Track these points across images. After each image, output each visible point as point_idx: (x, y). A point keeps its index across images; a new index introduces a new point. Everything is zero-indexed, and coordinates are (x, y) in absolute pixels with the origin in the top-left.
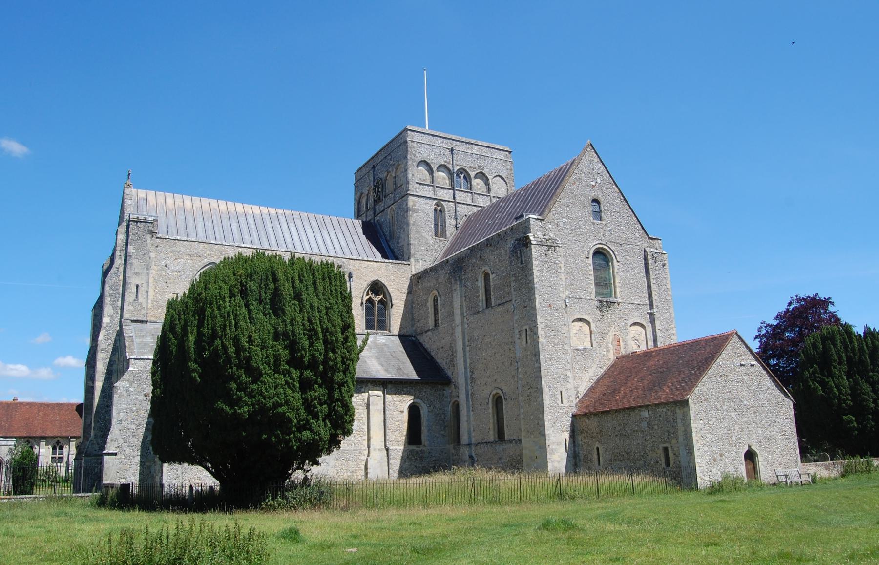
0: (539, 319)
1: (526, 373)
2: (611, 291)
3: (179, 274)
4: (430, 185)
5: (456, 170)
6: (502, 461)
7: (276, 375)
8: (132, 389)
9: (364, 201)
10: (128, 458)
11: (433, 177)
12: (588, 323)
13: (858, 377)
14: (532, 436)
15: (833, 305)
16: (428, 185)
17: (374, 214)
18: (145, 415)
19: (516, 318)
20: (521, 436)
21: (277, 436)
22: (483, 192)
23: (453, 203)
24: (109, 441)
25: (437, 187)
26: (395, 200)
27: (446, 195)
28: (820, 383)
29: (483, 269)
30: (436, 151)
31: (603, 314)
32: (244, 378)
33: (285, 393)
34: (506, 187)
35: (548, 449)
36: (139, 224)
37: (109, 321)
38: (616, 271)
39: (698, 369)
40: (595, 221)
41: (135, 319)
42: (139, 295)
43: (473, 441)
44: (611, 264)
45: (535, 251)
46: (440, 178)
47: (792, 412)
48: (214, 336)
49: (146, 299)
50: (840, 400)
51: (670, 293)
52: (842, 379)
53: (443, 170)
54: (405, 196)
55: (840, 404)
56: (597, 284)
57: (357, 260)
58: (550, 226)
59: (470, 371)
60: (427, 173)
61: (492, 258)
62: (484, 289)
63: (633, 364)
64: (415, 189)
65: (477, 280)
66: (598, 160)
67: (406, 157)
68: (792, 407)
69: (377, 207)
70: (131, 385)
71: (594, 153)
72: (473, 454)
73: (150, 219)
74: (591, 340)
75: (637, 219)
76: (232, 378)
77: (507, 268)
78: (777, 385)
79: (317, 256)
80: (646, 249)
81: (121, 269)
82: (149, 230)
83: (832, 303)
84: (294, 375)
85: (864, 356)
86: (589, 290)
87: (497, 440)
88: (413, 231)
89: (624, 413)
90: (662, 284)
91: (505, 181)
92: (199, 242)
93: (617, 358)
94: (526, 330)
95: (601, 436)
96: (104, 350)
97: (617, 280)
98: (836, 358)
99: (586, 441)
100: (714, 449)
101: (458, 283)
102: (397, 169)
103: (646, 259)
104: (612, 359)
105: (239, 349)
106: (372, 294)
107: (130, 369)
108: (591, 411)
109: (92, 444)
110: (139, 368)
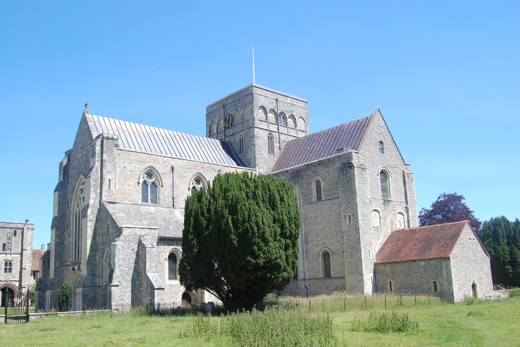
0: (359, 210)
1: (349, 239)
2: (388, 194)
3: (132, 173)
4: (266, 122)
5: (279, 113)
6: (329, 289)
7: (275, 242)
8: (125, 246)
9: (215, 127)
10: (125, 288)
11: (267, 117)
12: (379, 212)
13: (513, 245)
14: (353, 275)
15: (464, 199)
16: (265, 122)
17: (225, 135)
18: (133, 262)
19: (342, 208)
20: (345, 275)
21: (275, 275)
22: (292, 127)
23: (278, 133)
24: (114, 278)
25: (269, 123)
26: (243, 129)
27: (274, 128)
28: (492, 248)
29: (316, 178)
30: (268, 100)
31: (385, 207)
32: (262, 244)
33: (279, 252)
34: (304, 124)
35: (364, 282)
36: (109, 140)
37: (93, 202)
38: (391, 183)
39: (450, 240)
40: (382, 154)
41: (109, 201)
42: (111, 186)
43: (307, 277)
44: (388, 179)
45: (356, 171)
46: (270, 117)
47: (490, 264)
48: (244, 221)
49: (115, 189)
50: (504, 257)
51: (415, 196)
52: (505, 246)
53: (272, 112)
54: (252, 127)
55: (504, 260)
56: (382, 190)
57: (228, 167)
58: (361, 157)
59: (305, 237)
60: (263, 114)
61: (323, 172)
62: (316, 190)
63: (405, 236)
64: (258, 124)
66: (382, 119)
67: (252, 103)
68: (489, 261)
69: (227, 132)
70: (124, 244)
71: (380, 114)
72: (307, 285)
73: (115, 137)
74: (380, 222)
75: (400, 153)
76: (255, 244)
77: (334, 179)
78: (484, 250)
79: (207, 164)
80: (404, 170)
81: (99, 169)
82: (115, 144)
83: (464, 198)
84: (283, 242)
85: (516, 234)
86: (379, 193)
87: (325, 277)
89: (408, 263)
90: (412, 190)
91: (304, 120)
92: (143, 153)
93: (392, 232)
94: (350, 215)
95: (393, 275)
96: (91, 220)
97: (391, 188)
98: (501, 235)
99: (382, 278)
100: (460, 282)
101: (297, 185)
102: (244, 110)
103: (404, 176)
104: (390, 233)
106: (147, 177)
107: (123, 233)
108: (387, 261)
109: (86, 280)
110: (128, 233)
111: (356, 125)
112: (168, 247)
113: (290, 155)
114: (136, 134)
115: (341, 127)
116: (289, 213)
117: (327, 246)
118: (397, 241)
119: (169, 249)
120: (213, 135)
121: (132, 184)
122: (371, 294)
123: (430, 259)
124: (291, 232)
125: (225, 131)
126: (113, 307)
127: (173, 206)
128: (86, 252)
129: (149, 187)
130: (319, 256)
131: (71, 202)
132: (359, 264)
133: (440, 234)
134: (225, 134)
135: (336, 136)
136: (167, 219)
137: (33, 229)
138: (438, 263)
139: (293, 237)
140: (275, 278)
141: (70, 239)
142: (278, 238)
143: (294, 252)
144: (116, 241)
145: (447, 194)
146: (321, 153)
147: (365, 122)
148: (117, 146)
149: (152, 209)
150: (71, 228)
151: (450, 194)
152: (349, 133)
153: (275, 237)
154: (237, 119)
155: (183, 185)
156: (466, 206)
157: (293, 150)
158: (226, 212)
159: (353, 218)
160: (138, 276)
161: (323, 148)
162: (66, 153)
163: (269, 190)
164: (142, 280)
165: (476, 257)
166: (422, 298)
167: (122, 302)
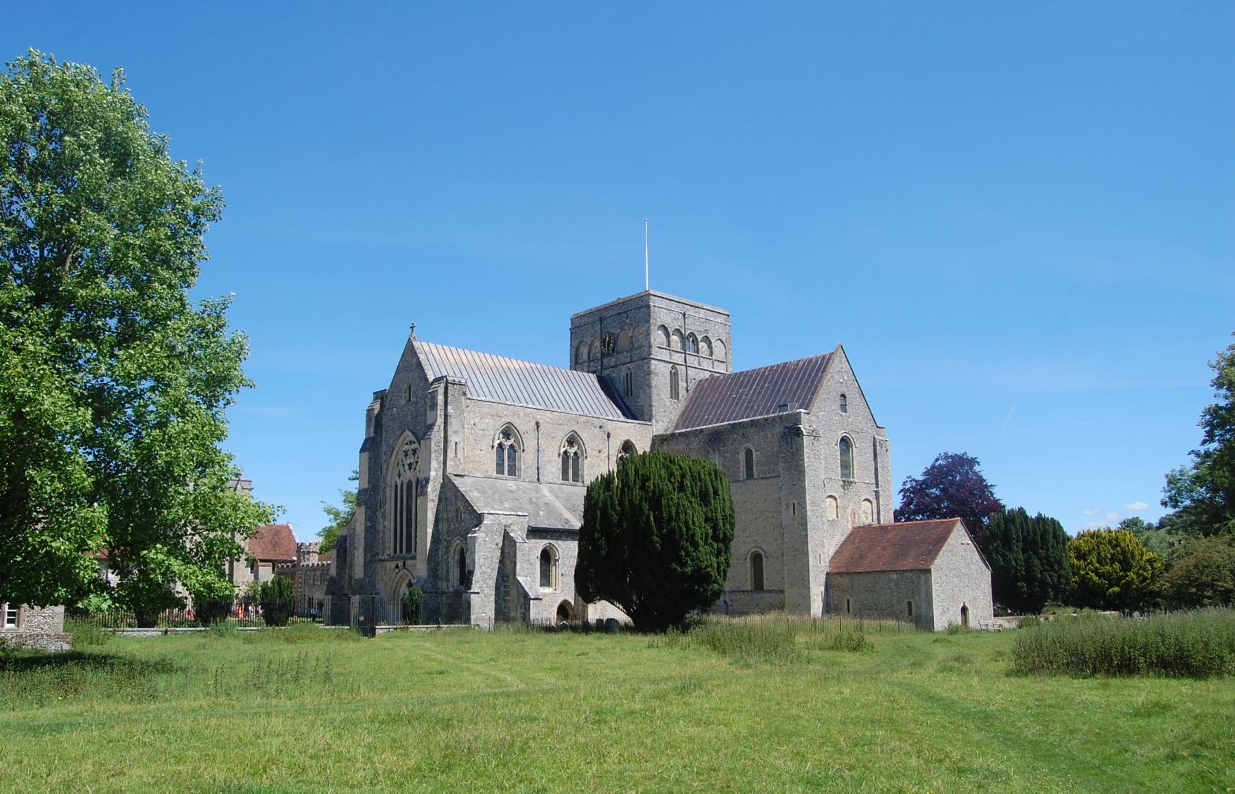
0: (808, 497)
8: (487, 539)
9: (584, 350)
11: (669, 341)
12: (835, 499)
17: (602, 365)
19: (784, 492)
21: (704, 588)
24: (473, 582)
27: (678, 358)
32: (691, 549)
38: (854, 455)
40: (843, 413)
41: (456, 473)
42: (458, 452)
47: (990, 580)
48: (670, 519)
50: (1016, 569)
55: (1016, 573)
65: (738, 454)
69: (605, 360)
72: (727, 600)
73: (463, 381)
76: (682, 548)
77: (773, 449)
78: (982, 559)
81: (442, 428)
83: (978, 463)
88: (654, 391)
96: (432, 500)
97: (855, 463)
101: (717, 453)
102: (634, 329)
103: (875, 445)
105: (688, 528)
107: (485, 522)
111: (808, 366)
112: (540, 540)
113: (704, 404)
114: (483, 370)
115: (784, 367)
116: (723, 510)
117: (760, 545)
118: (861, 541)
119: (542, 545)
120: (581, 364)
121: (484, 448)
122: (820, 616)
123: (904, 571)
124: (725, 534)
125: (602, 359)
126: (472, 622)
127: (538, 480)
128: (426, 545)
129: (506, 452)
130: (746, 559)
131: (388, 469)
132: (806, 573)
133: (922, 536)
134: (602, 363)
135: (777, 381)
136: (534, 500)
137: (250, 490)
138: (914, 577)
139: (726, 540)
140: (703, 592)
141: (386, 523)
142: (710, 541)
143: (727, 559)
144: (475, 532)
145: (950, 454)
146: (753, 406)
147: (821, 364)
148: (465, 394)
149: (511, 484)
150: (387, 506)
151: (956, 455)
152: (796, 378)
153: (706, 540)
154: (623, 342)
155: (551, 449)
156: (981, 477)
157: (709, 395)
158: (646, 506)
159: (799, 506)
160: (503, 580)
161: (757, 399)
162: (374, 393)
163: (700, 480)
164: (509, 586)
165: (971, 569)
166: (892, 623)
167: (483, 615)
